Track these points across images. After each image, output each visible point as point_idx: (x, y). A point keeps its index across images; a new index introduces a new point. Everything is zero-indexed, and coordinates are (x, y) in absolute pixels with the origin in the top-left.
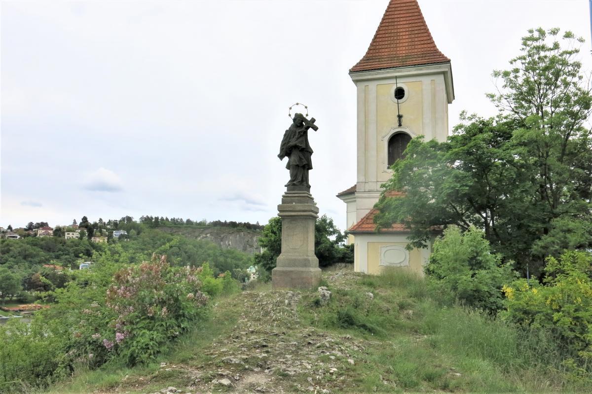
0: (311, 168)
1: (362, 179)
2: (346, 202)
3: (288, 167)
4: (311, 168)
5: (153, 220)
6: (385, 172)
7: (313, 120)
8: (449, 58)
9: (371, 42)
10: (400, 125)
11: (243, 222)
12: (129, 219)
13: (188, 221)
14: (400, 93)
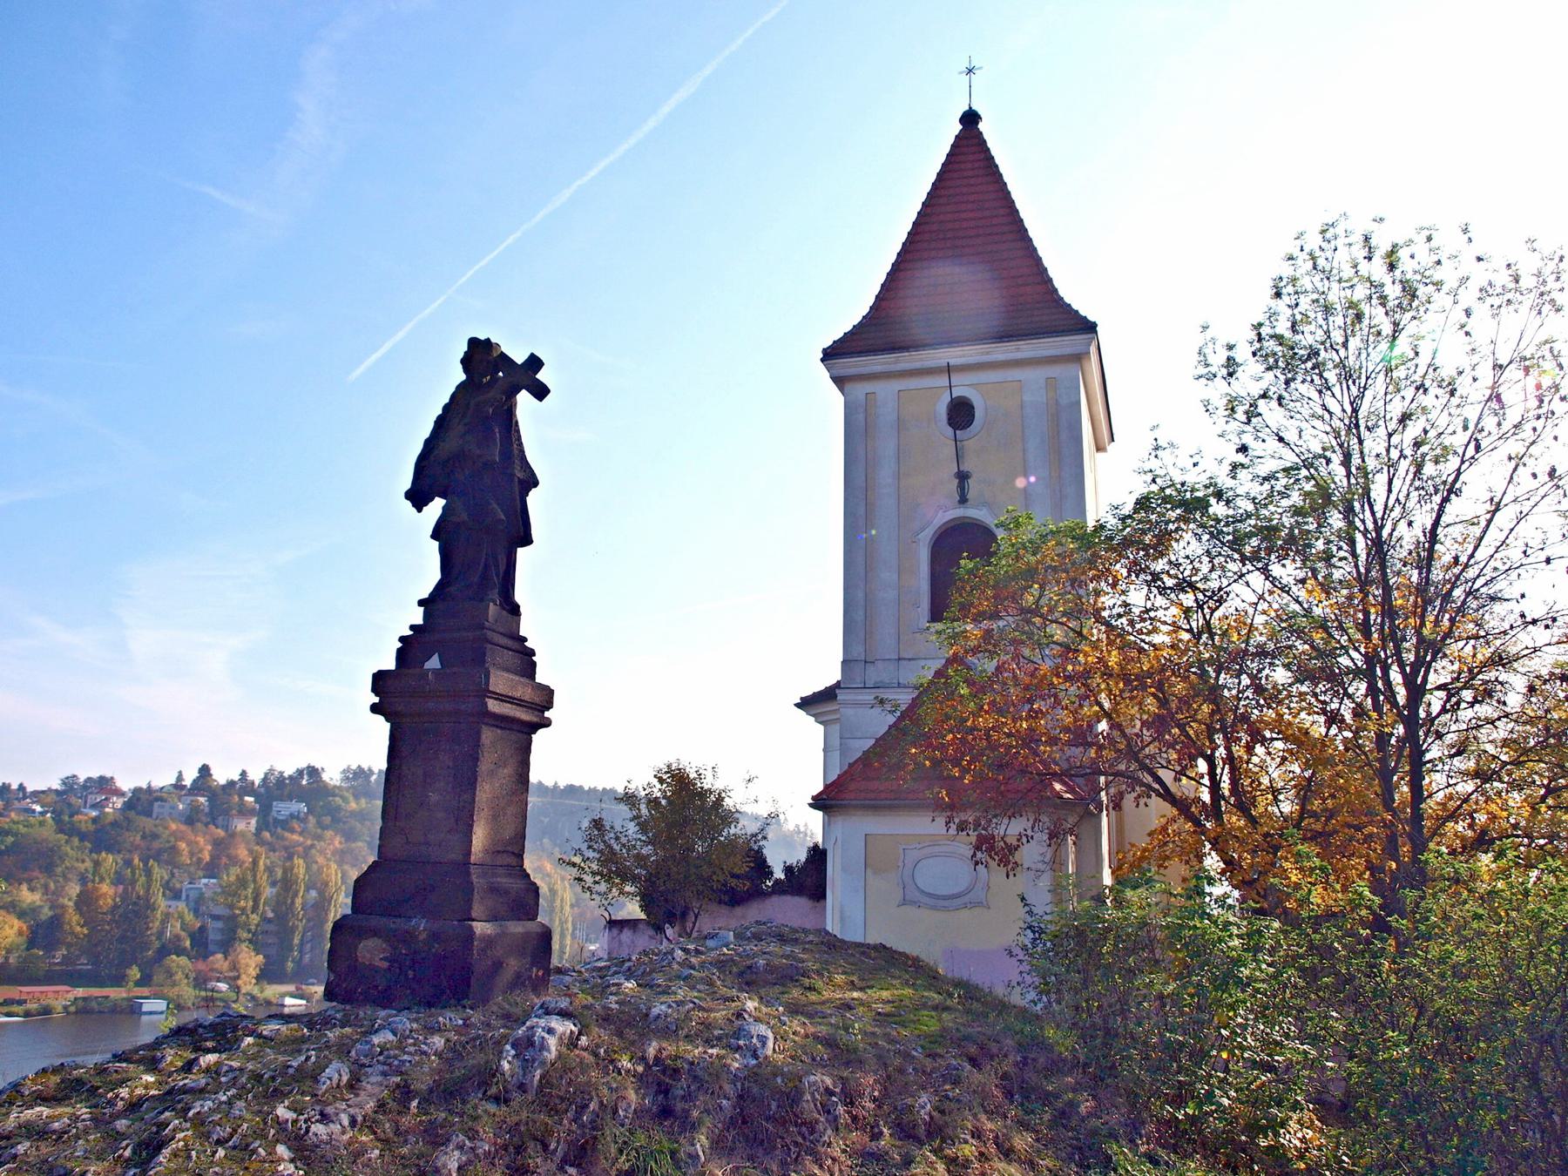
0: (527, 540)
4: (527, 540)
5: (374, 778)
7: (535, 363)
10: (963, 500)
11: (600, 788)
14: (961, 414)
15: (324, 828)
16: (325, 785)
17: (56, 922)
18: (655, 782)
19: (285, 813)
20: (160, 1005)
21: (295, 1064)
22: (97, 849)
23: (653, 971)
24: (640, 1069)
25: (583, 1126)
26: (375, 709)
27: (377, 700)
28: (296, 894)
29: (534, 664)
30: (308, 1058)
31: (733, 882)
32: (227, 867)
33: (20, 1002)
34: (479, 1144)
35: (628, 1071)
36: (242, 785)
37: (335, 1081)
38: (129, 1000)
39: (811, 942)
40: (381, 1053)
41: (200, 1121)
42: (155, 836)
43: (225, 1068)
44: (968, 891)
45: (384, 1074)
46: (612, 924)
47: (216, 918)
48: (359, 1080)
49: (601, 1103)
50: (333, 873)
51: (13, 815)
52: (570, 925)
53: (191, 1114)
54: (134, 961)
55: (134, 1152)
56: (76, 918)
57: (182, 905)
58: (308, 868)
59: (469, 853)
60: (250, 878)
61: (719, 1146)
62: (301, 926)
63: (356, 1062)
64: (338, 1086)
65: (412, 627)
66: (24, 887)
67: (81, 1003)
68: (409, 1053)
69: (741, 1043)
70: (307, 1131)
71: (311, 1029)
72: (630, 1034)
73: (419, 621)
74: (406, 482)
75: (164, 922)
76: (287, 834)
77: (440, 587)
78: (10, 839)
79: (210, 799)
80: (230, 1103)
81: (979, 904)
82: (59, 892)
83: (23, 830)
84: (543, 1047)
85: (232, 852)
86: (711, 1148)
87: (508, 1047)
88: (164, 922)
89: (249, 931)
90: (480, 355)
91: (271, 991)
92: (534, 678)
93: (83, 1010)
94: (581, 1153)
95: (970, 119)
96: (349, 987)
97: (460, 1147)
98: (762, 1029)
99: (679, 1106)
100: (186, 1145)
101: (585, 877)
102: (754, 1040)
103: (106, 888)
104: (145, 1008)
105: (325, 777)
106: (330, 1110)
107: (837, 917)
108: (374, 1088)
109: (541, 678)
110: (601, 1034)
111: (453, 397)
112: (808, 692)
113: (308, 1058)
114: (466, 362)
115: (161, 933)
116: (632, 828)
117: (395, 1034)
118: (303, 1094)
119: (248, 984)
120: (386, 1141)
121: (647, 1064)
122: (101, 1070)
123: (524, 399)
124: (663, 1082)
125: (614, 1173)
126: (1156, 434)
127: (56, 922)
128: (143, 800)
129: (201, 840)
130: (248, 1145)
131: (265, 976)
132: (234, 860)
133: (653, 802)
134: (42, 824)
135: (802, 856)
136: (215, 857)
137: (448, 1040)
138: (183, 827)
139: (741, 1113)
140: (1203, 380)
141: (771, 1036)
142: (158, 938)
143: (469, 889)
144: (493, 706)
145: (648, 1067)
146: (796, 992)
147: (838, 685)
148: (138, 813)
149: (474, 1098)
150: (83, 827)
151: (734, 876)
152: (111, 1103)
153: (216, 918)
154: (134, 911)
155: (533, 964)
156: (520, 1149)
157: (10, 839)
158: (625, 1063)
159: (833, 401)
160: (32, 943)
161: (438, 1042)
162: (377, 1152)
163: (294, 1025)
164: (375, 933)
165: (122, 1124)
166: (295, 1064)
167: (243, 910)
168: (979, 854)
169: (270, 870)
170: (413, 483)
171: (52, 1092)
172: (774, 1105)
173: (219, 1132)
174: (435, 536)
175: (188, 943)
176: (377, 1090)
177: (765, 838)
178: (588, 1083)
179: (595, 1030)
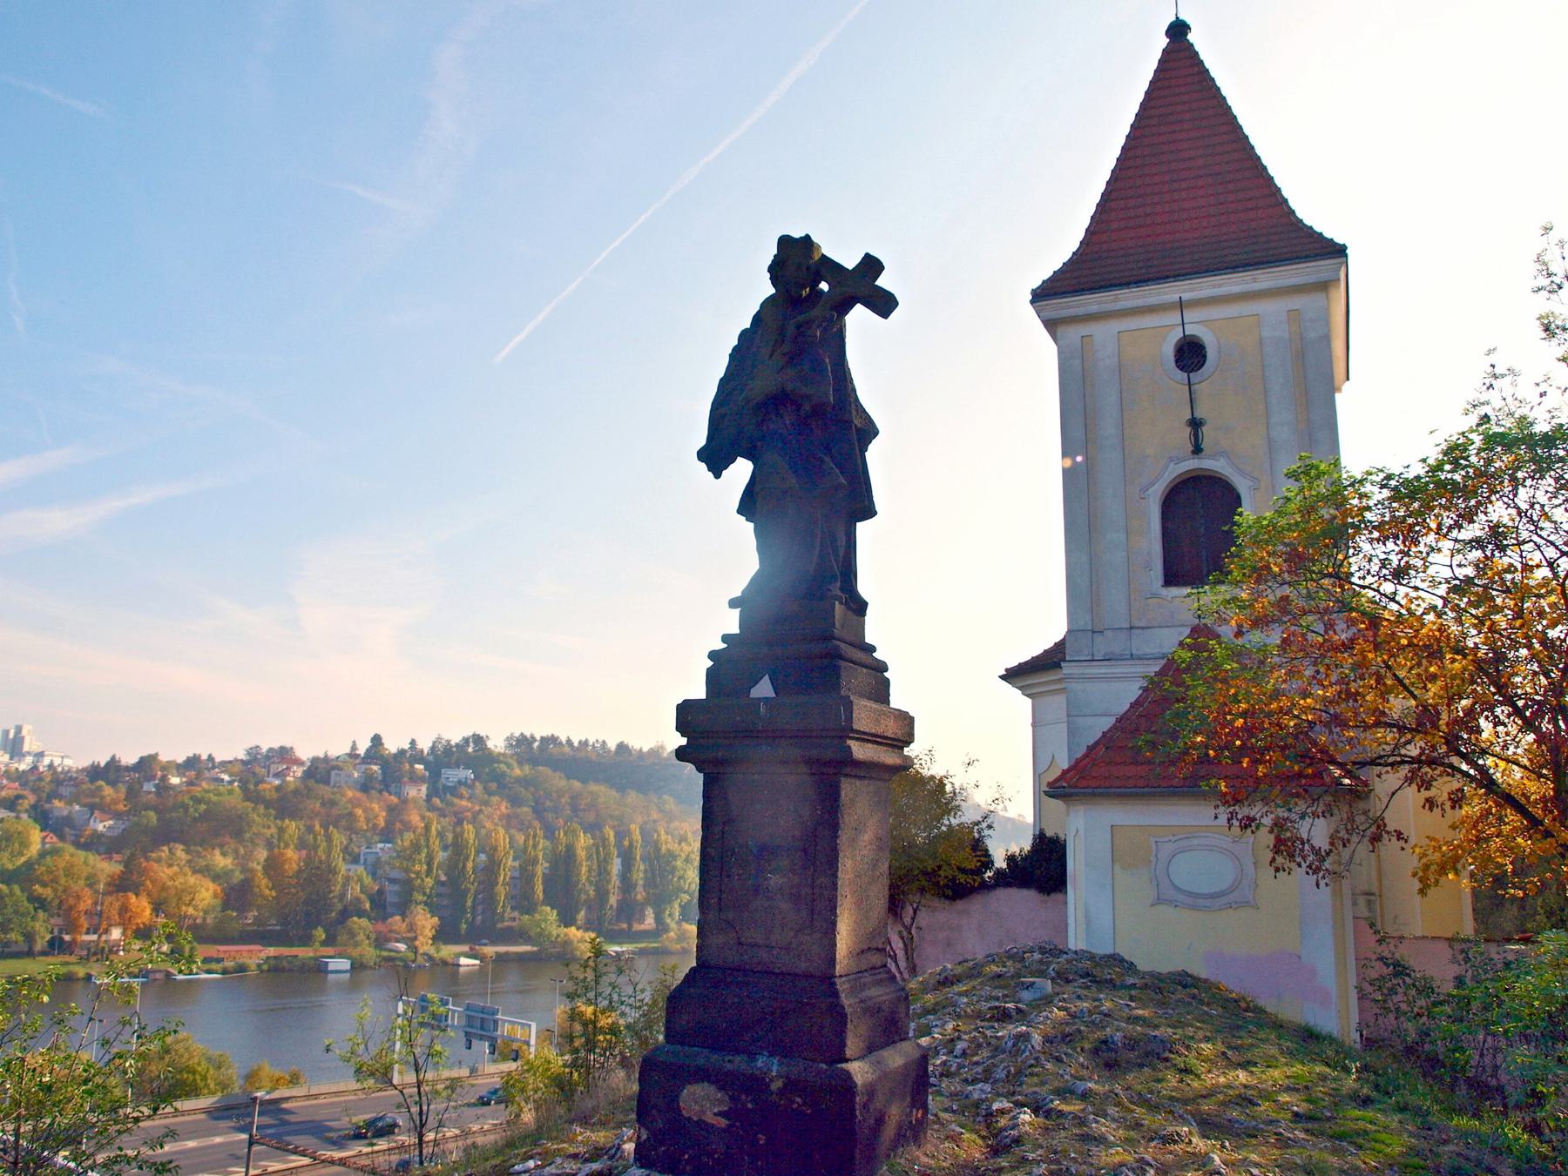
0: (869, 512)
1: (1085, 621)
3: (749, 505)
4: (869, 512)
6: (1155, 596)
7: (871, 266)
8: (1339, 240)
10: (1197, 450)
12: (479, 740)
13: (622, 747)
14: (1190, 354)
15: (490, 794)
16: (490, 752)
19: (454, 779)
20: (345, 964)
22: (281, 815)
27: (684, 741)
28: (467, 859)
29: (887, 682)
32: (401, 833)
33: (219, 960)
36: (412, 754)
38: (316, 959)
42: (333, 803)
44: (1230, 890)
47: (392, 881)
54: (319, 923)
56: (264, 882)
57: (360, 869)
59: (832, 961)
62: (473, 888)
65: (725, 638)
66: (217, 852)
67: (272, 962)
74: (701, 439)
75: (344, 885)
76: (456, 800)
78: (203, 807)
79: (384, 768)
81: (1246, 904)
82: (249, 856)
83: (215, 799)
85: (405, 818)
90: (797, 263)
91: (447, 951)
92: (888, 703)
93: (275, 969)
95: (1178, 30)
104: (331, 967)
105: (490, 744)
109: (897, 701)
112: (1013, 663)
114: (777, 270)
115: (342, 896)
119: (425, 945)
123: (858, 318)
126: (1493, 359)
128: (321, 770)
131: (441, 936)
132: (408, 827)
134: (230, 792)
138: (359, 795)
140: (1544, 294)
142: (341, 900)
144: (860, 751)
148: (317, 782)
150: (267, 795)
151: (962, 870)
153: (392, 881)
154: (317, 875)
159: (1045, 351)
160: (226, 905)
164: (702, 1075)
168: (1279, 860)
169: (441, 835)
170: (710, 438)
175: (368, 906)
177: (990, 827)
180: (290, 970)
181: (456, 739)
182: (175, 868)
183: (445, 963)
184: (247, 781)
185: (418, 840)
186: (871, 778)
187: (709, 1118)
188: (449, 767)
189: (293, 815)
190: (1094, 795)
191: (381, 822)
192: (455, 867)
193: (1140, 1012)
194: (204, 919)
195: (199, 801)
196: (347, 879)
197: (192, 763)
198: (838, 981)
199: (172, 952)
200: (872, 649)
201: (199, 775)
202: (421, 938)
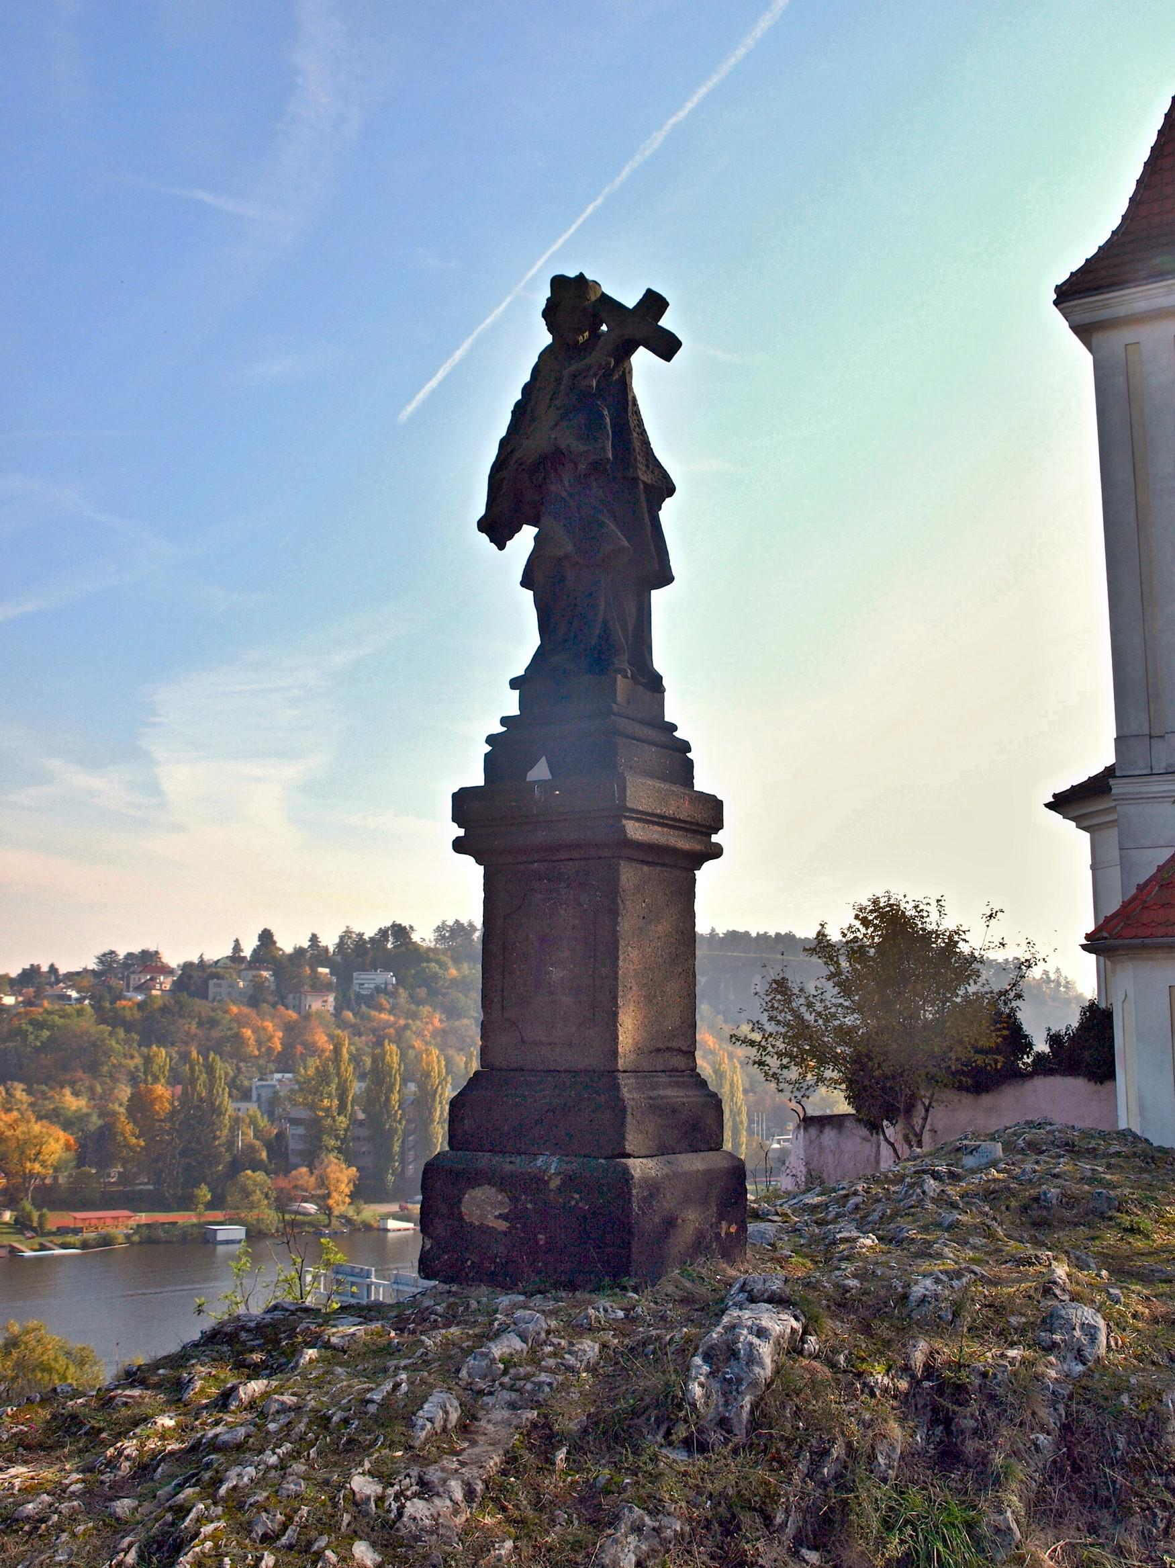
2: (1084, 829)
4: (665, 578)
7: (654, 303)
9: (1166, 111)
12: (400, 932)
15: (419, 1003)
17: (107, 1134)
18: (857, 924)
20: (238, 1232)
21: (377, 1397)
22: (146, 1041)
23: (896, 1214)
24: (903, 1385)
25: (824, 1484)
26: (459, 846)
27: (461, 832)
28: (391, 1089)
29: (690, 763)
30: (397, 1386)
31: (980, 1060)
32: (303, 1058)
34: (665, 1521)
35: (886, 1390)
36: (314, 953)
37: (438, 1424)
38: (201, 1226)
39: (1118, 1154)
40: (505, 1372)
41: (236, 1503)
42: (213, 1023)
43: (275, 1407)
45: (513, 1406)
46: (808, 1122)
47: (295, 1122)
48: (475, 1418)
49: (849, 1445)
50: (435, 1059)
51: (46, 1003)
52: (744, 1117)
53: (223, 1491)
55: (141, 1556)
56: (129, 1127)
57: (253, 1108)
58: (403, 1055)
59: (614, 1054)
60: (332, 1070)
61: (1041, 1510)
62: (400, 1128)
63: (469, 1387)
64: (444, 1429)
65: (504, 721)
66: (67, 1091)
67: (145, 1231)
68: (548, 1370)
69: (1057, 1337)
70: (400, 1514)
71: (400, 1330)
72: (883, 1329)
73: (514, 711)
74: (479, 508)
75: (233, 1130)
76: (373, 1013)
77: (540, 656)
78: (46, 1034)
79: (273, 971)
80: (282, 1466)
82: (108, 1095)
83: (60, 1022)
84: (753, 1359)
86: (1028, 1514)
87: (698, 1360)
88: (233, 1130)
89: (337, 1137)
90: (572, 303)
91: (370, 1212)
93: (148, 1239)
94: (824, 1529)
96: (450, 1254)
97: (637, 1529)
98: (1087, 1314)
99: (971, 1446)
100: (217, 1546)
101: (768, 1059)
102: (1077, 1333)
103: (160, 1089)
104: (221, 1236)
105: (415, 937)
106: (433, 1474)
107: (1134, 1109)
108: (499, 1423)
109: (702, 784)
110: (837, 1328)
111: (536, 371)
113: (397, 1386)
114: (551, 314)
115: (231, 1143)
116: (831, 991)
117: (524, 1340)
118: (392, 1446)
119: (340, 1203)
120: (520, 1523)
121: (913, 1377)
122: (106, 1401)
123: (642, 360)
124: (939, 1400)
125: (879, 1562)
127: (107, 1134)
128: (196, 978)
129: (269, 1025)
130: (310, 1543)
131: (362, 1192)
132: (312, 1049)
133: (855, 949)
134: (80, 1013)
135: (1072, 1020)
136: (288, 1046)
137: (604, 1346)
138: (246, 1010)
139: (1069, 1455)
141: (1101, 1324)
143: (620, 1110)
144: (635, 831)
145: (915, 1382)
146: (1111, 1238)
147: (1109, 772)
148: (192, 995)
149: (653, 1441)
152: (112, 1464)
153: (295, 1122)
154: (197, 1115)
155: (721, 1217)
156: (730, 1527)
157: (46, 1034)
158: (879, 1377)
159: (1079, 361)
160: (81, 1160)
161: (589, 1347)
162: (509, 1544)
163: (376, 1326)
165: (123, 1506)
166: (377, 1397)
167: (327, 1110)
169: (355, 1059)
171: (39, 1436)
172: (1121, 1442)
173: (266, 1523)
174: (526, 582)
175: (264, 1154)
176: (503, 1433)
177: (1019, 996)
178: (828, 1414)
179: (829, 1324)
180: (167, 1242)
181: (370, 932)
182: (15, 1114)
183: (368, 1227)
184: (101, 998)
185: (325, 1066)
186: (664, 865)
187: (491, 1222)
188: (363, 969)
189: (162, 1041)
190: (1145, 947)
191: (277, 1045)
192: (375, 1101)
193: (1108, 1177)
194: (55, 1178)
195: (39, 1025)
196: (237, 1121)
197: (30, 975)
198: (620, 1075)
199: (16, 1221)
200: (674, 728)
201: (39, 993)
202: (335, 1195)
